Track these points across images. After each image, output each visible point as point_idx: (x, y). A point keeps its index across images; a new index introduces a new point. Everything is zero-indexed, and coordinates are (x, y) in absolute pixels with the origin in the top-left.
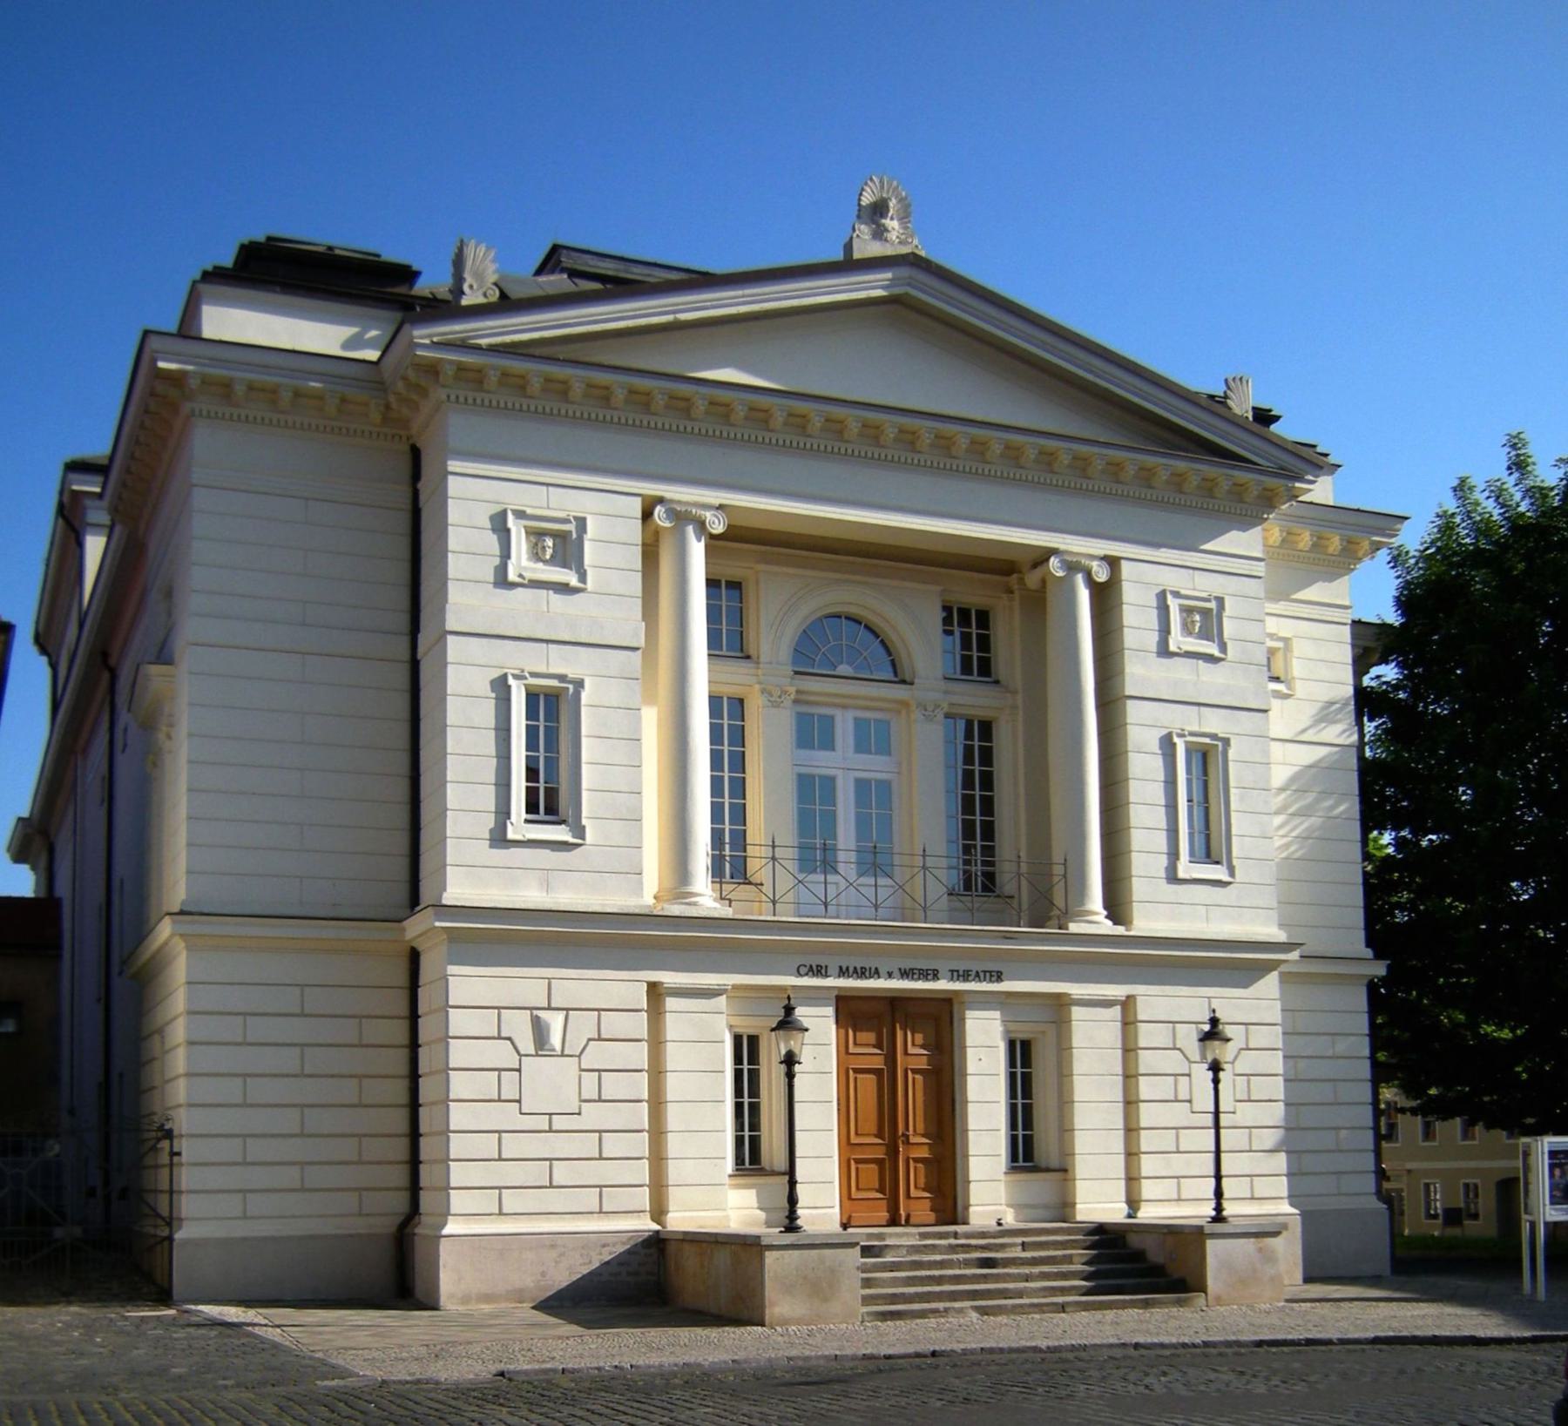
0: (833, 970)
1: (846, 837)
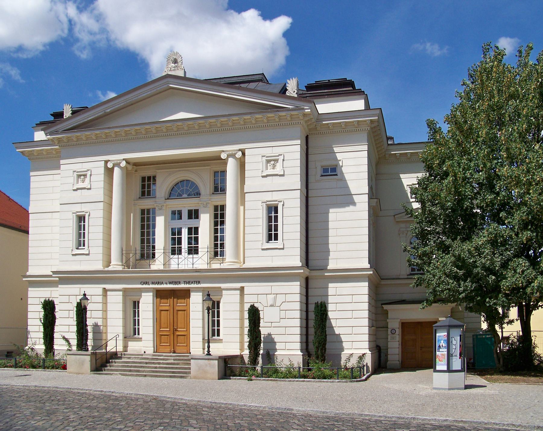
0: (150, 282)
1: (185, 245)
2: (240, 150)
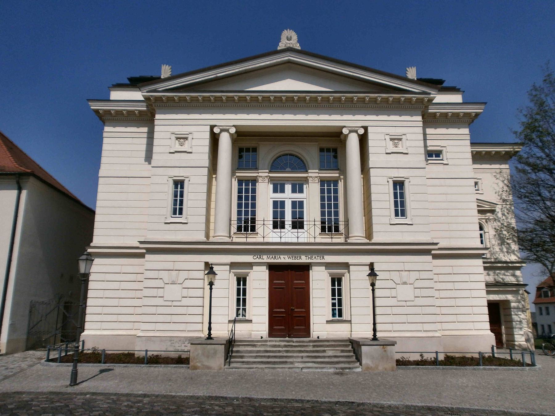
1: (288, 218)
2: (362, 127)
